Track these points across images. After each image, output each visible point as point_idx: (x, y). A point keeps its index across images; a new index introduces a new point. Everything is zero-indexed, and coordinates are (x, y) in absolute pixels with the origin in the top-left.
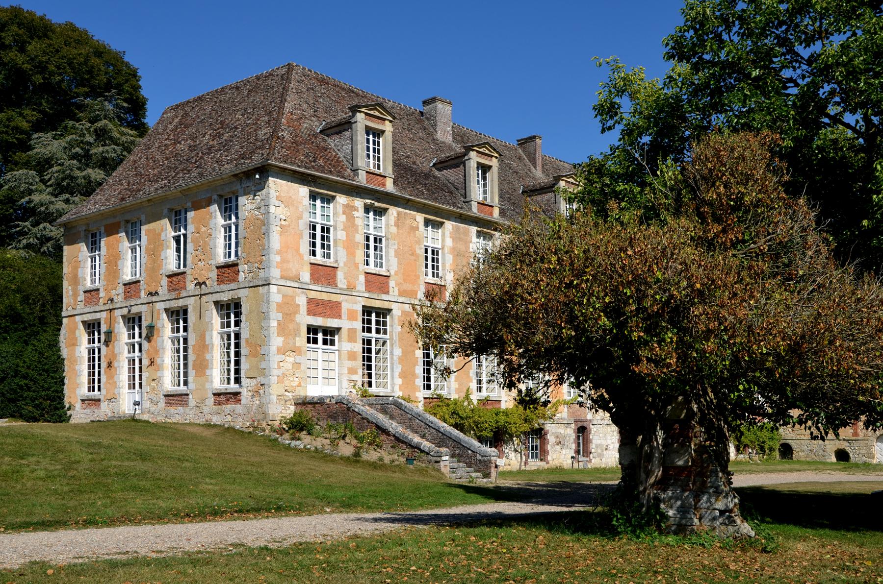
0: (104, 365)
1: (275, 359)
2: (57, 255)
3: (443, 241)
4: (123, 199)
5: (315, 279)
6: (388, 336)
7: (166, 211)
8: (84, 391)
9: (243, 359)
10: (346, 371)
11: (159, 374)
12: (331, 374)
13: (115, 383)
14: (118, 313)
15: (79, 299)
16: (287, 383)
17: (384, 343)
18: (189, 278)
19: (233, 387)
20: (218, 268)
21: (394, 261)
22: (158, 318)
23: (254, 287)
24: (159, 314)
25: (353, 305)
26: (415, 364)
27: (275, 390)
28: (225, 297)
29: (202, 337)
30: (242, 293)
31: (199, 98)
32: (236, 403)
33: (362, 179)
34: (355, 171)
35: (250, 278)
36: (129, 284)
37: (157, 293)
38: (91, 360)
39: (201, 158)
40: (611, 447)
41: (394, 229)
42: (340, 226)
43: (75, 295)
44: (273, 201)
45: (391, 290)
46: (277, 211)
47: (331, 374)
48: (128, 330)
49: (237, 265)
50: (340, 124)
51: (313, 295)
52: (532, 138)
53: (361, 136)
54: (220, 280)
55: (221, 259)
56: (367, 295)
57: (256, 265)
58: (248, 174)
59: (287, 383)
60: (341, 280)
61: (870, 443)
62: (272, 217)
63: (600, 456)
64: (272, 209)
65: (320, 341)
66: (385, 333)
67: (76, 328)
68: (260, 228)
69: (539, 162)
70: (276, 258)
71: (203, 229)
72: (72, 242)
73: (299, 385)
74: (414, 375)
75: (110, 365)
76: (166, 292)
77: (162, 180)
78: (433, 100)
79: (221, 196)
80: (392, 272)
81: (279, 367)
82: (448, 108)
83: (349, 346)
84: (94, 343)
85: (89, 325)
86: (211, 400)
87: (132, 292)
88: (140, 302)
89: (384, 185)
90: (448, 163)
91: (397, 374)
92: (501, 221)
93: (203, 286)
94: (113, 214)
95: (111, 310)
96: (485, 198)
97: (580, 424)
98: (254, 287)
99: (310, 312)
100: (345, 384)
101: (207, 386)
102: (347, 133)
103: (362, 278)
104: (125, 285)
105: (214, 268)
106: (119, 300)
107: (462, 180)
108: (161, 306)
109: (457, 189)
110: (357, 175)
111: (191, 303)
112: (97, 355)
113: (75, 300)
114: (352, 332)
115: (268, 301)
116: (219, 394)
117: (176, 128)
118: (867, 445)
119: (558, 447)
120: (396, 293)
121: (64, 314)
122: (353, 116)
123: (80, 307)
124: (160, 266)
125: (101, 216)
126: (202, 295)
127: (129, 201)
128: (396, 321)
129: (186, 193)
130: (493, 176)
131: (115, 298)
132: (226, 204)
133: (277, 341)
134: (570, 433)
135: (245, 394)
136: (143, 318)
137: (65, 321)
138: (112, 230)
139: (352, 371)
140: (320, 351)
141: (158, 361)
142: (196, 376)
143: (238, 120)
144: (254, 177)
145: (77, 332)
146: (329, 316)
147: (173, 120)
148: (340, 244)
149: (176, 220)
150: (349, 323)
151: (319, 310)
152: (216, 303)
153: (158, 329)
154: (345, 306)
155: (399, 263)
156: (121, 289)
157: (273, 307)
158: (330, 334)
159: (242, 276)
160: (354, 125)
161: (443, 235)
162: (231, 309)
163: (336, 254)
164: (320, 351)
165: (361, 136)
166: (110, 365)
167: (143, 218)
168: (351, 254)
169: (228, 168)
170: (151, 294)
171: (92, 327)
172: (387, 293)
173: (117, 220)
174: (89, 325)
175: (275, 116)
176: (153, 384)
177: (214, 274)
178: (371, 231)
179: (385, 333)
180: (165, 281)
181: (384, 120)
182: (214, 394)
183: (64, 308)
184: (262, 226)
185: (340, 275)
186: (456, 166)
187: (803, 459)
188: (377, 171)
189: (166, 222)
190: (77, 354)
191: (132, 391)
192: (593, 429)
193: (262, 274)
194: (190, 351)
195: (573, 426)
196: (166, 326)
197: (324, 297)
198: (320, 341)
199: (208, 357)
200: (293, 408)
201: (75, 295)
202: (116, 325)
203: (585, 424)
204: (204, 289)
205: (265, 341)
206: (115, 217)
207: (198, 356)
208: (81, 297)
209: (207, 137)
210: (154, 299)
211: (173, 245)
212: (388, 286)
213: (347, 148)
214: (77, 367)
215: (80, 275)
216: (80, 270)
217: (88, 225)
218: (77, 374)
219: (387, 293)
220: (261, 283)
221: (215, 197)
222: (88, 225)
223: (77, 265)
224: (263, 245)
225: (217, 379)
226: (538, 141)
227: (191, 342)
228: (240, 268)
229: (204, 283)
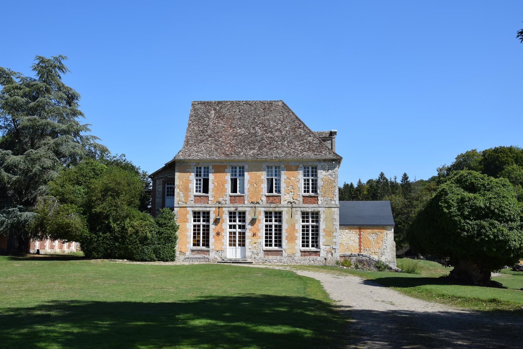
71: (293, 178)
95: (219, 207)
108: (263, 209)
135: (323, 254)
137: (175, 209)
159: (320, 202)
166: (218, 234)
202: (224, 215)
214: (187, 234)
216: (190, 185)
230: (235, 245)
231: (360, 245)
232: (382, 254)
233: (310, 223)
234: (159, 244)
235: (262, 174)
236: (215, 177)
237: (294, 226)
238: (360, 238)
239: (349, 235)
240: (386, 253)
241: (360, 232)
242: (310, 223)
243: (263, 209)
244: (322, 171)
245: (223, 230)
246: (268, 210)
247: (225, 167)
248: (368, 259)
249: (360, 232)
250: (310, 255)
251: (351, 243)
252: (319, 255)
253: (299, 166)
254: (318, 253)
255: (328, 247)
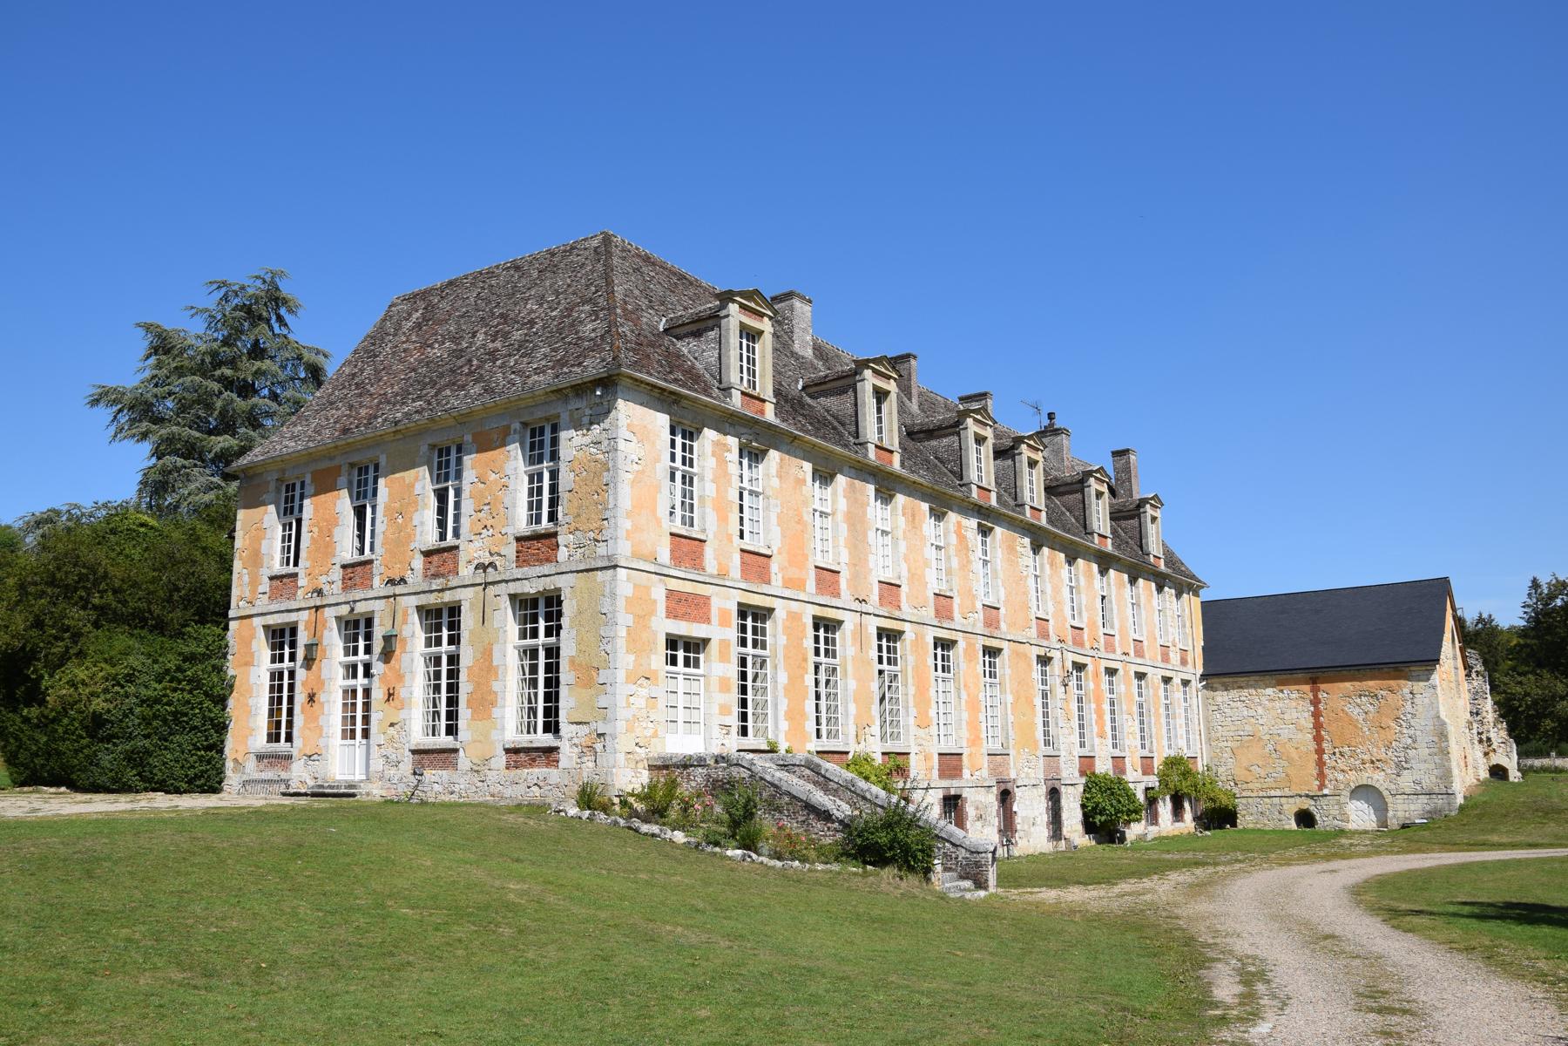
0: (300, 698)
1: (622, 689)
2: (226, 523)
3: (834, 502)
4: (345, 431)
5: (677, 559)
6: (836, 661)
7: (424, 449)
8: (260, 741)
9: (564, 691)
10: (716, 709)
11: (402, 715)
12: (695, 716)
13: (320, 728)
14: (330, 613)
15: (261, 589)
16: (638, 731)
17: (763, 663)
18: (463, 556)
19: (543, 739)
20: (518, 539)
21: (776, 532)
22: (405, 622)
23: (587, 571)
24: (405, 614)
25: (725, 602)
26: (805, 698)
27: (624, 743)
28: (530, 588)
29: (487, 654)
30: (560, 582)
31: (451, 283)
32: (548, 765)
33: (736, 401)
34: (726, 390)
35: (578, 556)
36: (353, 565)
37: (403, 581)
38: (276, 689)
39: (479, 367)
40: (1038, 821)
41: (775, 482)
42: (709, 475)
43: (254, 582)
44: (623, 433)
45: (773, 577)
46: (628, 449)
47: (695, 716)
48: (347, 640)
49: (555, 535)
50: (698, 320)
51: (674, 585)
52: (906, 357)
53: (734, 338)
54: (521, 560)
55: (522, 525)
56: (743, 586)
57: (592, 535)
58: (581, 389)
59: (638, 731)
60: (711, 563)
61: (1342, 799)
62: (620, 455)
63: (1028, 834)
64: (621, 445)
65: (680, 660)
66: (764, 647)
67: (253, 636)
68: (597, 475)
69: (914, 392)
70: (625, 524)
71: (493, 477)
72: (254, 503)
73: (655, 735)
74: (803, 715)
75: (311, 698)
76: (420, 578)
77: (414, 401)
78: (789, 296)
79: (525, 424)
80: (775, 549)
81: (629, 705)
82: (807, 308)
83: (719, 667)
84: (281, 661)
85: (274, 632)
86: (501, 760)
87: (358, 580)
88: (371, 594)
89: (762, 412)
90: (828, 386)
91: (781, 714)
92: (904, 472)
93: (490, 570)
94: (327, 454)
95: (317, 608)
96: (881, 439)
97: (1003, 787)
98: (587, 571)
99: (672, 614)
100: (716, 732)
101: (495, 735)
102: (712, 334)
103: (737, 557)
104: (344, 567)
105: (511, 539)
106: (335, 592)
107: (851, 411)
108: (414, 601)
109: (843, 425)
110: (730, 396)
111: (466, 597)
112: (286, 681)
113: (253, 591)
114: (724, 644)
115: (613, 595)
116: (516, 751)
117: (418, 326)
118: (1338, 803)
119: (979, 824)
120: (780, 583)
121: (231, 614)
122: (723, 306)
123: (263, 604)
124: (410, 538)
125: (310, 457)
126: (487, 584)
127: (356, 436)
128: (780, 628)
129: (463, 419)
130: (891, 405)
131: (326, 588)
132: (533, 436)
133: (625, 661)
134: (991, 799)
135: (568, 754)
136: (376, 621)
137: (232, 625)
138: (325, 484)
139: (724, 710)
140: (680, 677)
141: (402, 693)
142: (473, 719)
143: (532, 311)
144: (593, 395)
145: (254, 643)
146: (695, 620)
147: (410, 315)
148: (709, 504)
149: (440, 464)
150: (721, 632)
151: (681, 610)
152: (513, 597)
153: (404, 641)
154: (715, 604)
155: (784, 536)
156: (337, 574)
157: (621, 603)
158: (695, 646)
159: (562, 554)
160: (724, 322)
161: (834, 493)
162: (540, 610)
163: (703, 518)
164: (680, 677)
165: (734, 338)
166: (311, 698)
167: (383, 461)
168: (723, 519)
169: (542, 380)
170: (391, 582)
171: (281, 637)
172: (769, 583)
173: (336, 462)
174: (274, 632)
175: (602, 302)
176: (391, 731)
177: (511, 550)
178: (746, 484)
179: (764, 647)
180: (418, 562)
181: (762, 315)
182: (508, 751)
183: (233, 604)
184: (602, 475)
185: (709, 552)
186: (842, 391)
187: (1251, 826)
188: (750, 391)
189: (423, 472)
190: (252, 680)
191: (349, 742)
192: (1018, 793)
193: (601, 550)
194: (463, 677)
195: (994, 790)
196: (415, 635)
197: (688, 587)
198: (680, 660)
199: (496, 686)
200: (646, 773)
201: (254, 582)
202: (326, 633)
203: (1009, 786)
204: (492, 575)
205: (606, 661)
206: (331, 458)
207: (478, 685)
208: (265, 586)
209: (481, 336)
210: (399, 589)
211: (433, 502)
212: (769, 573)
213: (711, 356)
214: (251, 702)
215: (264, 550)
216: (264, 543)
217: (283, 471)
218: (249, 713)
219: (769, 583)
220: (600, 564)
221: (516, 425)
222: (283, 471)
223: (260, 533)
224: (604, 504)
225: (509, 720)
226: (913, 362)
227: (465, 663)
228: (560, 539)
229: (491, 564)
230: (353, 737)
231: (1318, 739)
232: (1400, 768)
233: (542, 638)
234: (146, 737)
235: (417, 479)
236: (316, 510)
237: (490, 655)
238: (1316, 715)
239: (1278, 704)
240: (1413, 763)
241: (1315, 691)
242: (542, 638)
243: (414, 601)
244: (572, 433)
245: (323, 684)
246: (431, 600)
247: (336, 471)
248: (745, 774)
249: (1315, 691)
250: (532, 762)
251: (1286, 732)
252: (455, 766)
253: (508, 427)
254: (554, 755)
255: (584, 730)
